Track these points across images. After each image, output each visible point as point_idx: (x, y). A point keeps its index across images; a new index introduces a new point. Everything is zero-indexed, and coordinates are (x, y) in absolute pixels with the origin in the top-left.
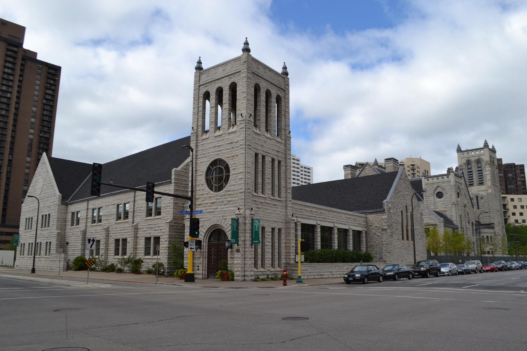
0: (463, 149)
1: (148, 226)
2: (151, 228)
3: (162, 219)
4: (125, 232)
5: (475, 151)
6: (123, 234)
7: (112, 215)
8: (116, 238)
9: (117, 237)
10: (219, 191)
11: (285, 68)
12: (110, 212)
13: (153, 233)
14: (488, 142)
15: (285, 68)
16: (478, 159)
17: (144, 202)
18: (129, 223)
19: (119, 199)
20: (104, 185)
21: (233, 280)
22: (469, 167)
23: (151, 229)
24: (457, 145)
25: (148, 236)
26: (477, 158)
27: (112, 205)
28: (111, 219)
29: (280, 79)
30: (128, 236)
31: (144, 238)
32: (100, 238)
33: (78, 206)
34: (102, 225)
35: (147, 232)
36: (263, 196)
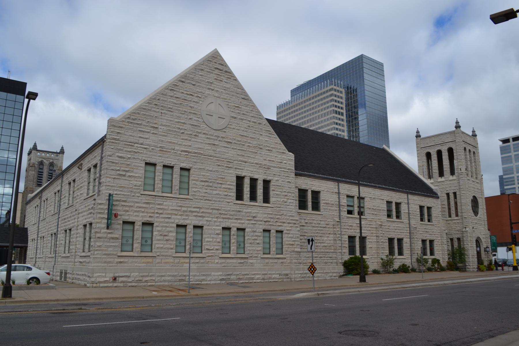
0: (39, 148)
1: (424, 230)
2: (426, 232)
3: (435, 226)
4: (401, 232)
5: (41, 152)
6: (399, 233)
7: (381, 211)
8: (390, 237)
9: (391, 236)
10: (478, 214)
11: (474, 131)
12: (379, 207)
13: (428, 237)
14: (37, 145)
15: (474, 131)
16: (52, 162)
17: (417, 207)
18: (405, 224)
19: (389, 196)
20: (8, 97)
21: (465, 271)
22: (41, 167)
23: (427, 233)
24: (61, 146)
25: (425, 239)
26: (51, 161)
27: (380, 199)
28: (380, 215)
29: (472, 139)
30: (205, 223)
31: (421, 240)
32: (367, 235)
33: (315, 184)
34: (368, 219)
35: (424, 235)
36: (450, 219)
